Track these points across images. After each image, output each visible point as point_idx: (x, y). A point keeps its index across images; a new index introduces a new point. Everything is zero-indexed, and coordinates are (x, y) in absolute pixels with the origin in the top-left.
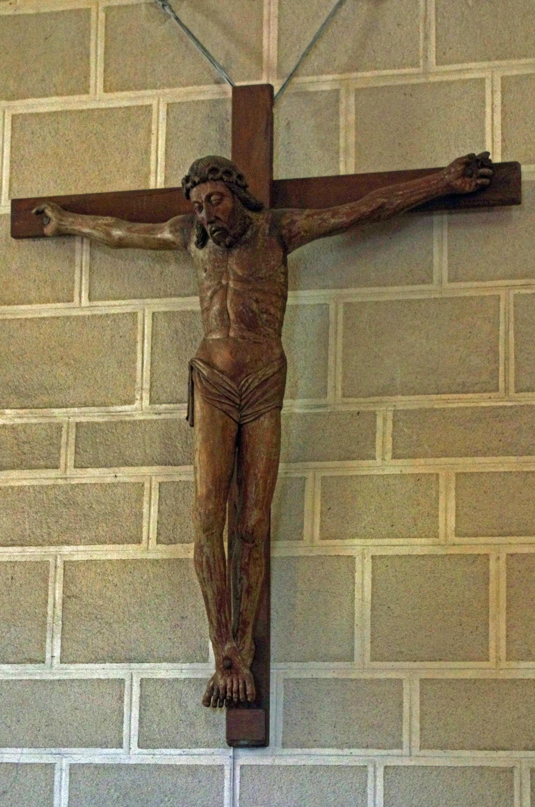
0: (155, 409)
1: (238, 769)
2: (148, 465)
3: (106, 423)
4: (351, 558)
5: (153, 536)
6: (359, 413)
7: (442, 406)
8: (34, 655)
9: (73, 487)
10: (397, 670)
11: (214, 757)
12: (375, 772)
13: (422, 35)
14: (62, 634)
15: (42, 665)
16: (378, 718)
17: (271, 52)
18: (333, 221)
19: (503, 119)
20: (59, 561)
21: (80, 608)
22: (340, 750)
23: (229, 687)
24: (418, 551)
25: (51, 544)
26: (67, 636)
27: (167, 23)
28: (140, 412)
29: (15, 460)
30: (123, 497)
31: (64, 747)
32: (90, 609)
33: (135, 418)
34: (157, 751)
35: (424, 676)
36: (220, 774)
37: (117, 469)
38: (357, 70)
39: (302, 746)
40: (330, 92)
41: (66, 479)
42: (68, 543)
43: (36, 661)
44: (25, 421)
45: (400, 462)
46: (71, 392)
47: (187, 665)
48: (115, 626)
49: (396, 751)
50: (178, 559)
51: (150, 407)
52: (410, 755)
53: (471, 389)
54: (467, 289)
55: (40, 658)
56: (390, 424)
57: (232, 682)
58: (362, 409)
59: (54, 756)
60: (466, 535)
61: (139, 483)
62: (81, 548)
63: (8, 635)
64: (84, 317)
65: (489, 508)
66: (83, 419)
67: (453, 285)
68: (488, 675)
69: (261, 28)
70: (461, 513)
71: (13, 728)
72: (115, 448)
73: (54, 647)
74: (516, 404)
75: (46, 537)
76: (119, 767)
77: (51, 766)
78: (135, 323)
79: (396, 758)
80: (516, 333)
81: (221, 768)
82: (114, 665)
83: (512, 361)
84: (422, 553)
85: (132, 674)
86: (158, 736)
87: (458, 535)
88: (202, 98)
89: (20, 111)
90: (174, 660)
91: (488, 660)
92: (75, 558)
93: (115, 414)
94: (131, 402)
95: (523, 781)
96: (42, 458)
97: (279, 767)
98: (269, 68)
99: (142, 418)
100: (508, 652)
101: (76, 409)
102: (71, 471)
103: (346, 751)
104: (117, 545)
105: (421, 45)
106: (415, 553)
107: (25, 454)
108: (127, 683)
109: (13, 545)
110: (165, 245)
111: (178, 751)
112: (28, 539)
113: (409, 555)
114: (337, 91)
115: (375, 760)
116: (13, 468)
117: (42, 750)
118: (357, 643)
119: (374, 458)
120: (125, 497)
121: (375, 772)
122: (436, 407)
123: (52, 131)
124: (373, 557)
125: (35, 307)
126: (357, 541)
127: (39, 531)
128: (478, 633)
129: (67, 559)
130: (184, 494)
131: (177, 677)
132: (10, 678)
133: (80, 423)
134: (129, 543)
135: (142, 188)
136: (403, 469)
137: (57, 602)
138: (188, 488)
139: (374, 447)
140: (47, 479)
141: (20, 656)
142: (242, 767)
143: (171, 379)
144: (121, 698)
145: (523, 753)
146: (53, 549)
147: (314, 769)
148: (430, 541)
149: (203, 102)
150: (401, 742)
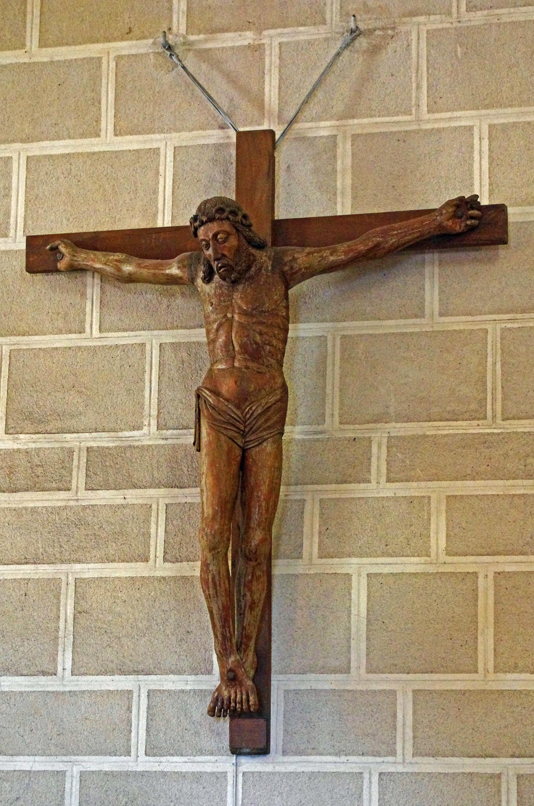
3: (116, 447)
4: (348, 577)
7: (433, 433)
8: (47, 667)
9: (84, 508)
11: (217, 764)
13: (414, 85)
14: (73, 647)
15: (55, 677)
17: (273, 99)
18: (332, 258)
19: (490, 164)
20: (70, 578)
32: (99, 624)
34: (163, 759)
38: (353, 117)
41: (77, 500)
42: (79, 561)
44: (38, 445)
47: (193, 677)
48: (125, 641)
49: (390, 759)
55: (53, 670)
57: (236, 693)
58: (359, 435)
59: (66, 764)
60: (456, 554)
61: (146, 504)
63: (22, 649)
66: (94, 444)
68: (479, 686)
73: (65, 660)
75: (58, 556)
76: (127, 774)
77: (63, 773)
81: (224, 774)
82: (122, 677)
85: (140, 685)
88: (207, 142)
90: (179, 672)
91: (476, 672)
98: (271, 114)
99: (151, 443)
101: (87, 434)
102: (82, 494)
103: (343, 758)
105: (414, 95)
108: (135, 695)
109: (27, 563)
110: (173, 280)
111: (185, 759)
112: (41, 557)
114: (335, 136)
115: (373, 766)
116: (27, 490)
119: (369, 481)
122: (428, 433)
126: (354, 560)
128: (467, 647)
132: (23, 689)
133: (91, 447)
134: (137, 561)
139: (369, 471)
142: (244, 773)
144: (129, 709)
146: (65, 567)
147: (312, 775)
148: (423, 559)
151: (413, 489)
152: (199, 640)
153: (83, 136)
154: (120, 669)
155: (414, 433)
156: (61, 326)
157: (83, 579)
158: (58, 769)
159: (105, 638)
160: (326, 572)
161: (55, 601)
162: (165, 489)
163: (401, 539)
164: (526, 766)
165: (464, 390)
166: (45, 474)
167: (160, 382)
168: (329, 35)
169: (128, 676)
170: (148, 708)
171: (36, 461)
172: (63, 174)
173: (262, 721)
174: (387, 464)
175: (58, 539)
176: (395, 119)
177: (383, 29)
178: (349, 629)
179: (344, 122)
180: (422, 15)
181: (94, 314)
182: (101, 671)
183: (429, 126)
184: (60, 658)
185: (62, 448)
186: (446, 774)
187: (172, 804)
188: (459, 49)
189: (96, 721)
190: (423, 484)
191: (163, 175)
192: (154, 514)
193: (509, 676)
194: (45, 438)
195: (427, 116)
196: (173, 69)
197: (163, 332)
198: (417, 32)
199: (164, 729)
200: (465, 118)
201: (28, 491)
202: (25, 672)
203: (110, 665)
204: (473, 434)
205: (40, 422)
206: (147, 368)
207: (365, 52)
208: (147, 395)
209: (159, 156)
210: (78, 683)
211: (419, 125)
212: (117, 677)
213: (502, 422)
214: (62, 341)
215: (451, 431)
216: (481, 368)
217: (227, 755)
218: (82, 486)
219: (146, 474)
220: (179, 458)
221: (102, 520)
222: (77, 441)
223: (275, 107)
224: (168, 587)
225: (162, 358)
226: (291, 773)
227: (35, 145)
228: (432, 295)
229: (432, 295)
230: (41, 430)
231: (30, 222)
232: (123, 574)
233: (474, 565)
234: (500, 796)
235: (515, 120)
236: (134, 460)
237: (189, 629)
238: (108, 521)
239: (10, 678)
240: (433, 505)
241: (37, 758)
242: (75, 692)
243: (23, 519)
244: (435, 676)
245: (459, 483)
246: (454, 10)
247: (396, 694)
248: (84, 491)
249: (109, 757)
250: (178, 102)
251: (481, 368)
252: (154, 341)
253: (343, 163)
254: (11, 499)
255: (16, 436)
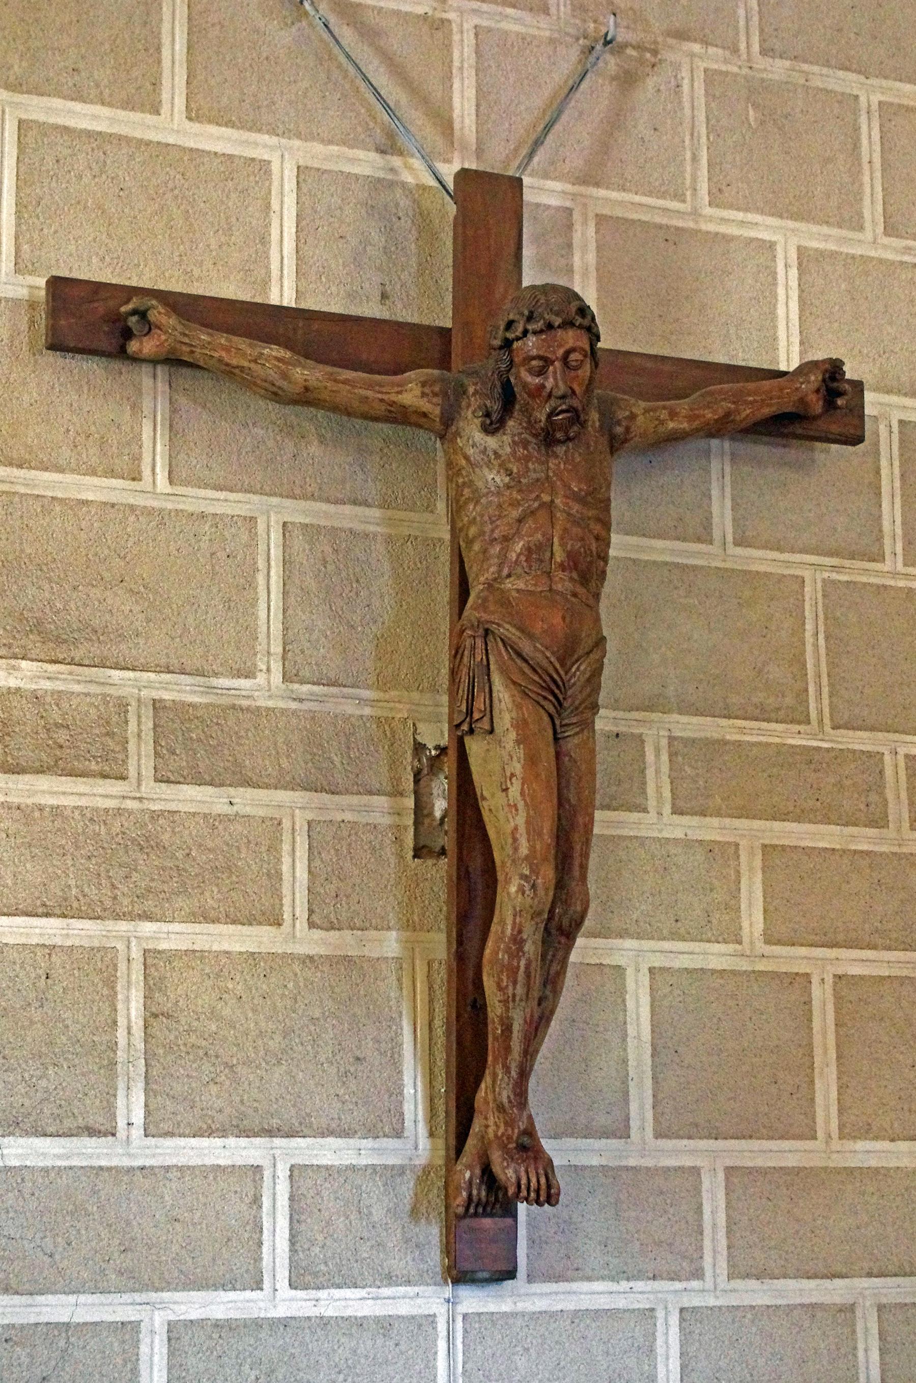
0: (292, 691)
1: (459, 1319)
2: (285, 788)
3: (207, 706)
4: (619, 970)
5: (302, 911)
6: (617, 735)
7: (737, 737)
8: (97, 1120)
9: (155, 816)
10: (692, 1152)
11: (419, 1301)
12: (666, 1319)
13: (688, 155)
14: (147, 1083)
15: (110, 1138)
16: (668, 1231)
17: (467, 121)
18: (671, 425)
19: (802, 310)
20: (134, 948)
21: (176, 1037)
22: (615, 1284)
23: (524, 1181)
24: (715, 963)
25: (118, 917)
26: (155, 1087)
27: (294, 30)
28: (267, 694)
29: (44, 756)
30: (245, 840)
31: (157, 1290)
32: (193, 1039)
33: (258, 704)
34: (323, 1294)
35: (729, 1163)
36: (430, 1330)
37: (231, 790)
38: (597, 185)
39: (558, 1278)
40: (558, 209)
41: (140, 799)
42: (147, 917)
43: (100, 1132)
44: (60, 686)
45: (686, 820)
46: (142, 641)
47: (369, 1143)
48: (241, 1070)
49: (695, 1284)
50: (346, 957)
51: (284, 686)
52: (716, 1288)
53: (773, 715)
54: (762, 560)
55: (108, 1126)
56: (665, 757)
57: (527, 1172)
58: (622, 729)
59: (138, 1307)
60: (779, 942)
61: (271, 819)
62: (176, 927)
63: (43, 1083)
64: (161, 510)
65: (807, 900)
66: (167, 696)
67: (739, 551)
68: (817, 1162)
69: (450, 78)
70: (771, 908)
71: (57, 1257)
72: (226, 752)
73: (132, 1106)
74: (834, 746)
75: (108, 903)
76: (257, 1324)
77: (133, 1327)
78: (253, 535)
79: (697, 1295)
80: (827, 638)
81: (431, 1319)
82: (243, 1141)
83: (825, 680)
84: (720, 968)
85: (275, 1157)
86: (323, 1267)
87: (768, 942)
88: (356, 170)
89: (34, 117)
90: (346, 1133)
91: (814, 1138)
92: (163, 946)
93: (219, 691)
94: (249, 674)
95: (869, 1325)
96: (94, 757)
97: (523, 1314)
98: (464, 148)
99: (271, 704)
100: (841, 1127)
101: (152, 675)
102: (149, 787)
103: (624, 1285)
104: (240, 927)
105: (688, 168)
106: (710, 967)
107: (61, 747)
108: (267, 1174)
109: (47, 915)
110: (400, 416)
111: (362, 1293)
112: (75, 905)
113: (702, 969)
114: (569, 211)
115: (665, 1297)
116: (40, 771)
117: (115, 1298)
118: (634, 1107)
119: (645, 810)
120: (249, 842)
121: (666, 1319)
122: (728, 737)
123: (94, 165)
124: (651, 970)
125: (69, 478)
126: (629, 943)
127: (95, 892)
128: (799, 1095)
129: (150, 947)
130: (350, 845)
131: (354, 1162)
132: (49, 1163)
133: (161, 701)
134: (260, 924)
135: (259, 300)
136: (689, 832)
137: (133, 1024)
138: (356, 834)
139: (644, 792)
140: (106, 796)
141: (68, 1123)
142: (465, 1316)
143: (318, 640)
144: (257, 1201)
145: (866, 1282)
146: (123, 926)
147: (577, 1315)
148: (731, 948)
149: (357, 177)
150: (702, 1269)
151: (711, 829)
152: (377, 1075)
153: (128, 105)
154: (238, 1126)
155: (709, 735)
156: (94, 460)
157: (159, 952)
158: (125, 1319)
159: (207, 1067)
160: (587, 961)
161: (105, 992)
162: (303, 793)
163: (698, 912)
164: (893, 1289)
165: (775, 672)
166: (79, 745)
167: (285, 593)
168: (556, 35)
169: (252, 1139)
170: (292, 1198)
171: (55, 716)
172: (91, 168)
173: (509, 1221)
174: (671, 783)
175: (108, 871)
176: (661, 203)
177: (638, 47)
178: (625, 1061)
179: (582, 189)
180: (695, 41)
181: (159, 447)
182: (200, 1128)
183: (711, 227)
184: (121, 1102)
185: (105, 696)
186: (778, 1307)
187: (341, 1377)
188: (751, 112)
189: (194, 1224)
190: (727, 821)
191: (278, 213)
192: (286, 837)
193: (860, 1145)
194: (70, 673)
195: (708, 211)
196: (293, 23)
197: (288, 502)
198: (692, 67)
199: (320, 1238)
200: (764, 227)
201: (43, 772)
202: (51, 1129)
203: (219, 1117)
204: (792, 746)
205: (59, 641)
206: (261, 564)
207: (613, 79)
208: (262, 614)
209: (270, 175)
210: (158, 1151)
211: (697, 222)
212: (232, 1141)
213: (832, 732)
214: (95, 489)
215: (762, 739)
216: (795, 639)
217: (435, 1284)
218: (148, 772)
219: (267, 762)
220: (325, 736)
221: (190, 842)
222: (133, 687)
223: (472, 138)
224: (319, 974)
225: (288, 551)
226: (540, 1313)
227: (35, 100)
228: (722, 507)
229: (722, 507)
230: (61, 657)
231: (26, 247)
232: (237, 947)
233: (805, 961)
234: (855, 1340)
235: (834, 248)
236: (242, 733)
237: (358, 1053)
238: (200, 845)
239: (22, 1141)
240: (743, 858)
241: (83, 1298)
242: (152, 1168)
243: (37, 828)
244: (755, 1144)
245: (777, 825)
246: (743, 46)
247: (699, 1174)
248: (152, 783)
249: (222, 1293)
250: (305, 84)
251: (795, 639)
252: (273, 518)
253: (582, 258)
254: (10, 785)
255: (13, 662)
